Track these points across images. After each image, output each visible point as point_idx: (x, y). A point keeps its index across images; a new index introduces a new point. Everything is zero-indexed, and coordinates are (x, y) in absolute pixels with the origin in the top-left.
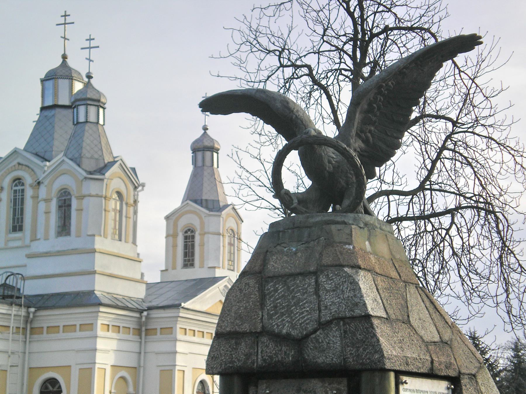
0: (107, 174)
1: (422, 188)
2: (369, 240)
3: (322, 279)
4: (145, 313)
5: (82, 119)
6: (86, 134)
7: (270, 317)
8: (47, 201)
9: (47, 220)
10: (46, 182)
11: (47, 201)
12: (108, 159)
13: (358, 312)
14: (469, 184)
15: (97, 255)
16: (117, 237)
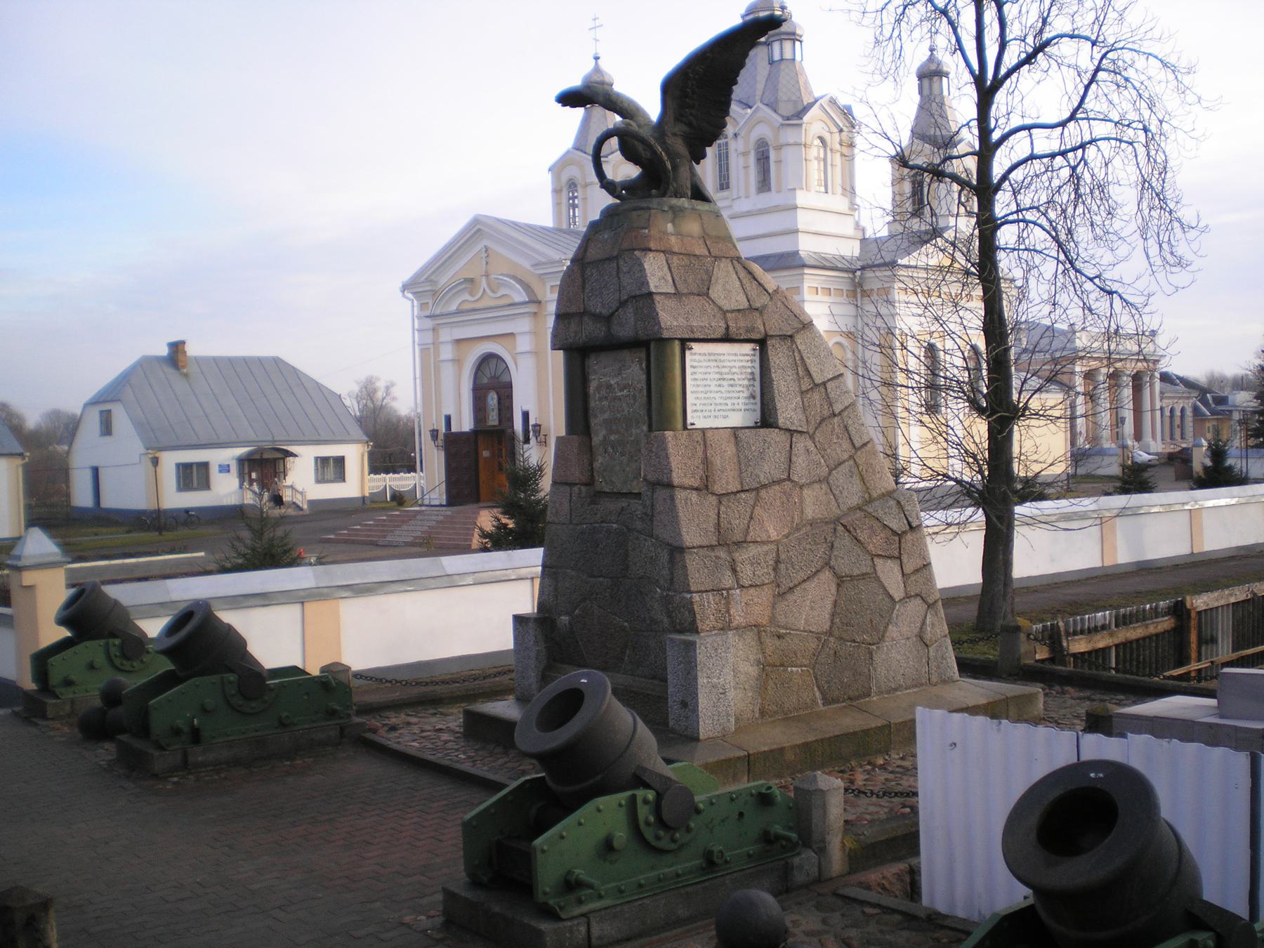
0: (806, 118)
1: (1072, 117)
2: (673, 222)
3: (621, 263)
4: (858, 273)
5: (777, 57)
6: (782, 74)
7: (589, 298)
8: (745, 154)
9: (747, 176)
10: (743, 133)
11: (745, 154)
12: (807, 100)
13: (644, 291)
14: (1124, 104)
15: (799, 211)
16: (823, 189)
